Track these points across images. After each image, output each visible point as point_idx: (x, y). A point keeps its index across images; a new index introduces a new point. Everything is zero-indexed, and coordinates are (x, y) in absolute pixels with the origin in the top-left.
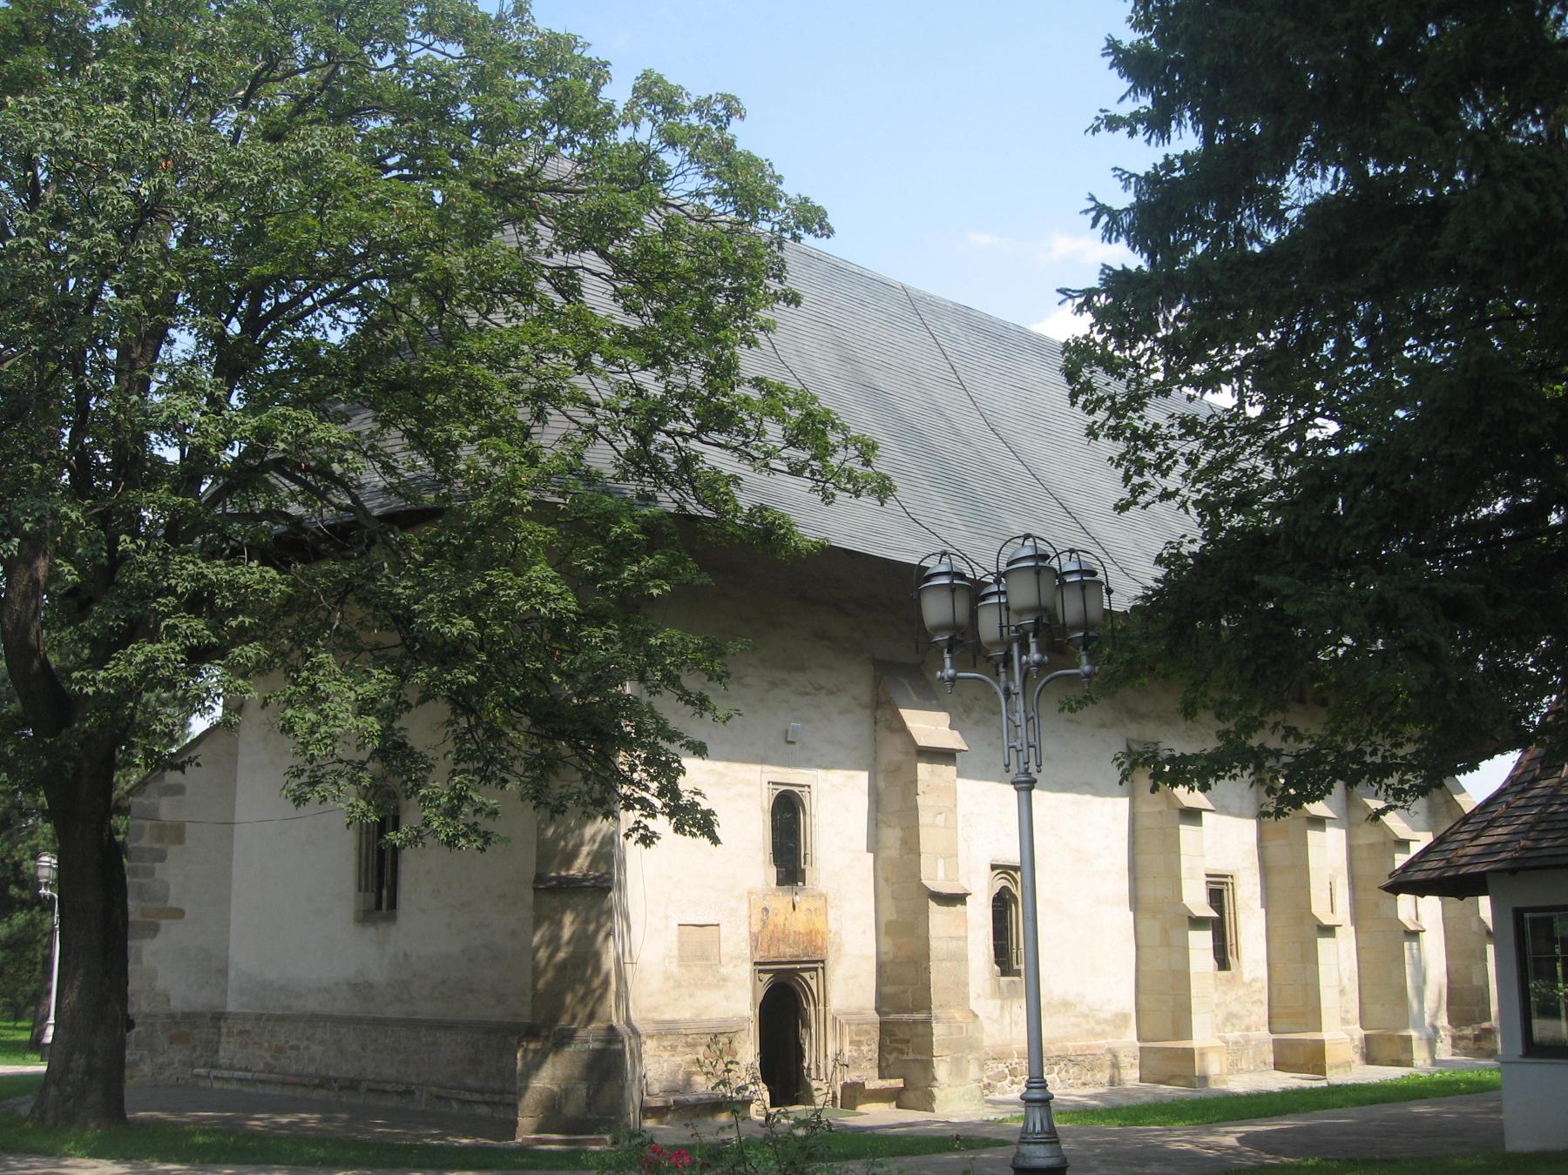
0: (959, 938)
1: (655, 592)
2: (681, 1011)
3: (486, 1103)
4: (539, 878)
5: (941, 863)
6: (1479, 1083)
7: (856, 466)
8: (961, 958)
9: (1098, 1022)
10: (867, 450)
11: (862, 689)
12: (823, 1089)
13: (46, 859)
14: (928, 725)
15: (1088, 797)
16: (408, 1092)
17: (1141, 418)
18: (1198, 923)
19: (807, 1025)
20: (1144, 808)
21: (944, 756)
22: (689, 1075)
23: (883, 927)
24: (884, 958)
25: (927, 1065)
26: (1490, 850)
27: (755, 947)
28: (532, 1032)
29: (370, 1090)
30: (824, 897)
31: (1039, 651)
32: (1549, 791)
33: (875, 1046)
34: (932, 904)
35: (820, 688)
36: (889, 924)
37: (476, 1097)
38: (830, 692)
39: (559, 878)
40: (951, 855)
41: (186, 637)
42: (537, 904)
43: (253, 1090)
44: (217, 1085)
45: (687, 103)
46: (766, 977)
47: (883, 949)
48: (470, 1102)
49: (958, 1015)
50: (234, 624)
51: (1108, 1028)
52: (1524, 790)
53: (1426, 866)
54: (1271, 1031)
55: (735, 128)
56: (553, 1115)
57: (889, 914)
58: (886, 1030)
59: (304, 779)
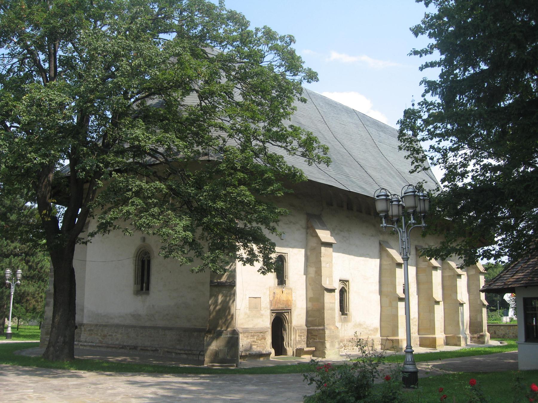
0: (333, 303)
1: (279, 195)
2: (249, 325)
3: (186, 354)
4: (211, 282)
5: (328, 279)
6: (486, 351)
7: (321, 154)
8: (333, 309)
9: (369, 331)
10: (325, 150)
11: (303, 222)
12: (290, 351)
13: (8, 270)
14: (325, 235)
15: (368, 259)
16: (156, 350)
17: (417, 145)
18: (401, 300)
19: (285, 330)
20: (384, 263)
21: (329, 245)
22: (251, 346)
23: (308, 300)
24: (309, 309)
25: (323, 343)
26: (517, 280)
27: (271, 305)
28: (209, 332)
29: (142, 349)
30: (291, 289)
31: (414, 219)
32: (534, 263)
33: (305, 337)
34: (325, 292)
35: (291, 222)
36: (311, 298)
37: (183, 352)
38: (294, 224)
39: (218, 282)
40: (331, 276)
41: (137, 205)
42: (211, 290)
43: (95, 349)
44: (81, 347)
45: (278, 37)
46: (274, 314)
47: (309, 306)
48: (179, 354)
49: (333, 328)
50: (151, 201)
51: (372, 332)
52: (526, 262)
53: (497, 284)
54: (419, 334)
55: (293, 46)
56: (216, 357)
57: (311, 295)
58: (309, 332)
59: (167, 250)
